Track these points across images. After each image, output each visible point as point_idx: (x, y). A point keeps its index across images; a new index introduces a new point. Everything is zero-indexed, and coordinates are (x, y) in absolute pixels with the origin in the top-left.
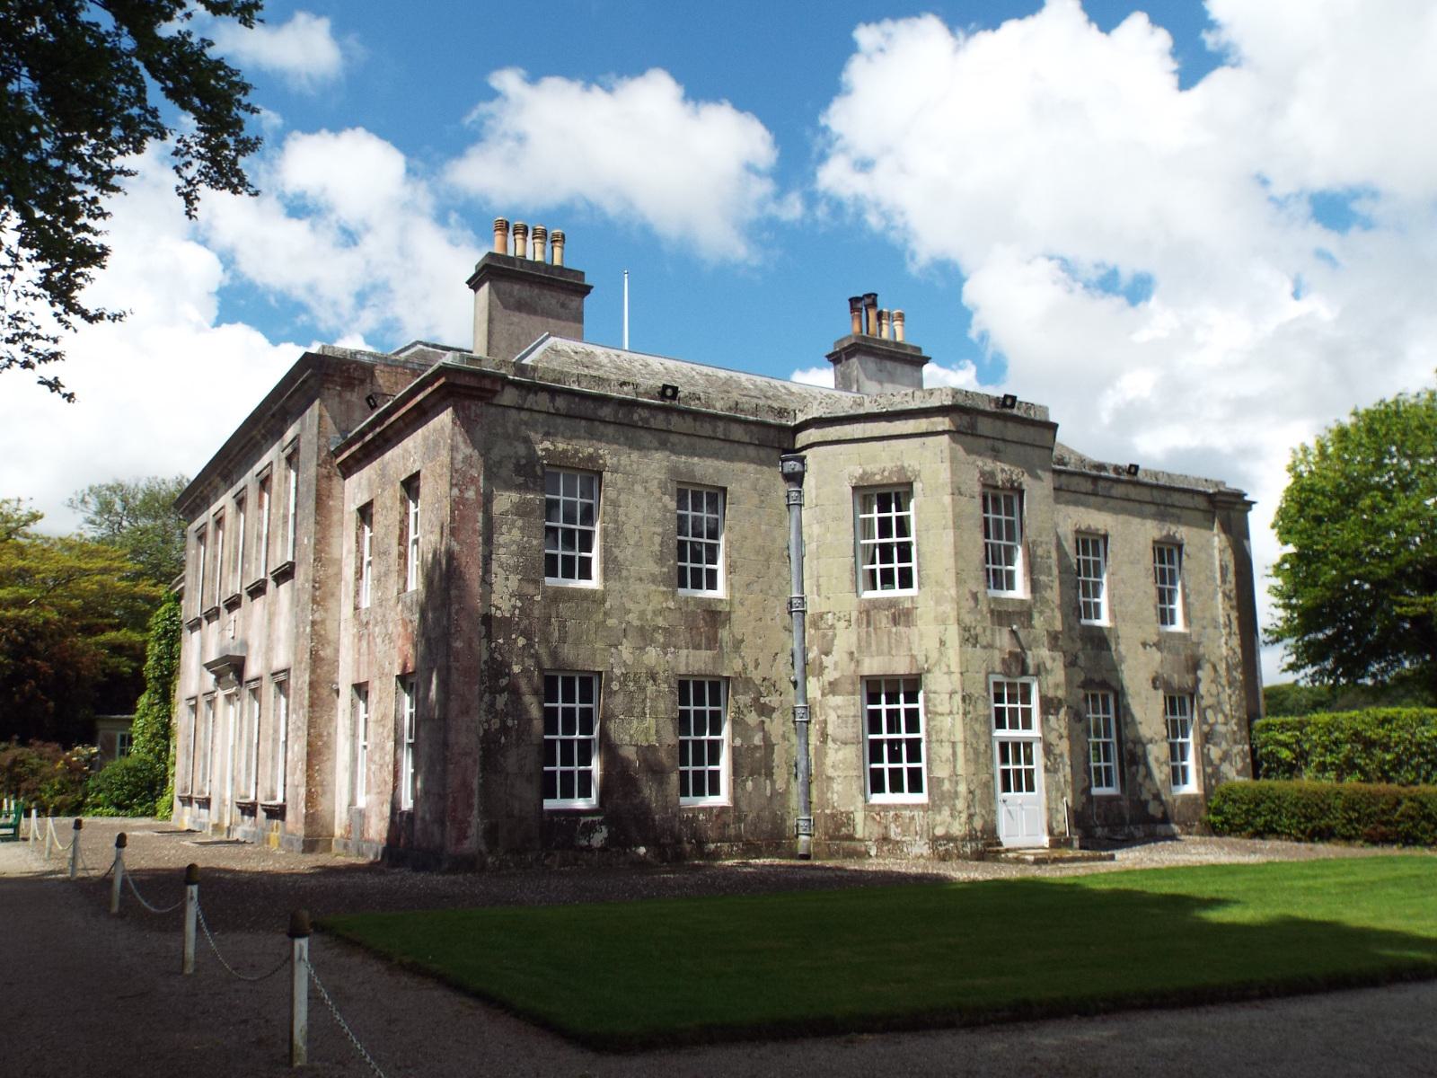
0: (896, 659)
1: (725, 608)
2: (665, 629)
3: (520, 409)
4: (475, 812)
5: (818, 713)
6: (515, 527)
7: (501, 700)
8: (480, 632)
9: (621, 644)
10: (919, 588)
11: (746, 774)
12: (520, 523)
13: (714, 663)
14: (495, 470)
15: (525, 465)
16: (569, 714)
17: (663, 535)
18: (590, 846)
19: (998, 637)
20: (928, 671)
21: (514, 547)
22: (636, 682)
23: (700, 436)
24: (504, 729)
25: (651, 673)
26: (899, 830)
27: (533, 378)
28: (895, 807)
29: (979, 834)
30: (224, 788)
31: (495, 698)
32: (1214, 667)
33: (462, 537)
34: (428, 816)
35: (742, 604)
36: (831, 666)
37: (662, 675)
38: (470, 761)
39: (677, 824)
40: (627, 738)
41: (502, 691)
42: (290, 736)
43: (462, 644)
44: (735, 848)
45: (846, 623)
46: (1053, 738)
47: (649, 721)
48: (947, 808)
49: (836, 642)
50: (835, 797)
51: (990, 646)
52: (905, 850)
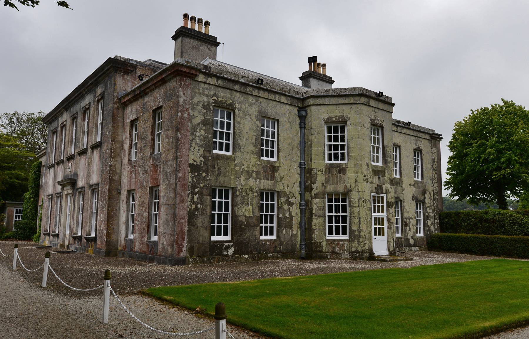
0: (340, 186)
1: (277, 165)
2: (256, 172)
3: (205, 83)
4: (185, 241)
5: (310, 205)
6: (202, 129)
7: (196, 197)
8: (188, 170)
9: (240, 177)
10: (348, 160)
11: (283, 228)
12: (204, 128)
13: (273, 185)
14: (195, 106)
15: (206, 105)
16: (220, 203)
17: (256, 136)
18: (228, 254)
19: (374, 180)
20: (351, 191)
21: (202, 137)
22: (245, 192)
23: (270, 100)
24: (197, 209)
25: (251, 189)
26: (339, 249)
27: (210, 71)
28: (337, 240)
29: (367, 251)
30: (56, 229)
31: (194, 196)
32: (430, 193)
33: (182, 132)
34: (165, 243)
35: (283, 164)
36: (315, 188)
37: (255, 190)
38: (184, 221)
39: (259, 246)
40: (242, 213)
41: (196, 194)
42: (99, 210)
43: (181, 175)
44: (279, 255)
45: (321, 173)
46: (390, 216)
47: (250, 207)
48: (356, 241)
49: (317, 179)
50: (316, 236)
51: (372, 183)
52: (341, 256)
